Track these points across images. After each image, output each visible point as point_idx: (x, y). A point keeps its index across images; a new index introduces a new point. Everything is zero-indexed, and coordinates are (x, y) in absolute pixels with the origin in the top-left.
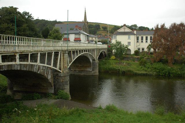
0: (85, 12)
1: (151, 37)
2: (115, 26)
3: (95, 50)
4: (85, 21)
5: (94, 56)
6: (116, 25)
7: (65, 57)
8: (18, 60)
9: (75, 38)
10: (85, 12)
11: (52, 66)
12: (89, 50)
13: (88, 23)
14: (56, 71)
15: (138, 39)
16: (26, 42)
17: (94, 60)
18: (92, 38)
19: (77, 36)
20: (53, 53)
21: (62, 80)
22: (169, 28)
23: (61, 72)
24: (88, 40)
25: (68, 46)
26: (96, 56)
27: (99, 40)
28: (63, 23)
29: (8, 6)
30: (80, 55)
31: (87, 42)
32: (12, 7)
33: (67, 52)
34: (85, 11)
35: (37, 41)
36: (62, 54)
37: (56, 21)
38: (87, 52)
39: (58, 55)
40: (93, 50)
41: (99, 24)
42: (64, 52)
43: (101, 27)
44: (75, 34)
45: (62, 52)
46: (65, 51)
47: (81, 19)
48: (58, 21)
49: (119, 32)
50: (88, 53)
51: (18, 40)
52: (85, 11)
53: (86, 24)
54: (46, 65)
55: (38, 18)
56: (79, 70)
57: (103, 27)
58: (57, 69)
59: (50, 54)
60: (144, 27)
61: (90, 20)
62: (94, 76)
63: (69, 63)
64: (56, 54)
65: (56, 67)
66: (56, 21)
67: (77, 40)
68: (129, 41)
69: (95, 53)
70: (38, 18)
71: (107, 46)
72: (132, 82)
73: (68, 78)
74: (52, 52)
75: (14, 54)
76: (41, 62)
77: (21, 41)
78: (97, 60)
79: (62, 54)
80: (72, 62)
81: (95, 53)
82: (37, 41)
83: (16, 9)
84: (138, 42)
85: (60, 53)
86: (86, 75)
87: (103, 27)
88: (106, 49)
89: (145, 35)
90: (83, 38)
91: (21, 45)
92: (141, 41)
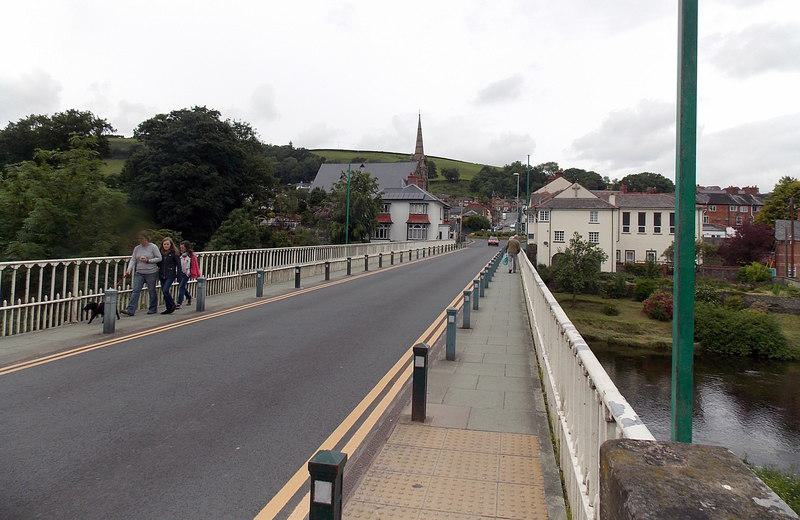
0: (420, 129)
1: (672, 215)
2: (486, 168)
9: (412, 216)
10: (420, 129)
15: (626, 219)
16: (789, 255)
19: (419, 210)
29: (189, 106)
32: (204, 109)
37: (290, 146)
44: (412, 202)
47: (411, 150)
48: (296, 146)
49: (562, 200)
57: (444, 172)
60: (583, 171)
61: (429, 151)
66: (290, 146)
67: (418, 223)
68: (594, 228)
83: (215, 113)
84: (626, 230)
86: (621, 345)
87: (444, 172)
89: (651, 208)
92: (653, 227)
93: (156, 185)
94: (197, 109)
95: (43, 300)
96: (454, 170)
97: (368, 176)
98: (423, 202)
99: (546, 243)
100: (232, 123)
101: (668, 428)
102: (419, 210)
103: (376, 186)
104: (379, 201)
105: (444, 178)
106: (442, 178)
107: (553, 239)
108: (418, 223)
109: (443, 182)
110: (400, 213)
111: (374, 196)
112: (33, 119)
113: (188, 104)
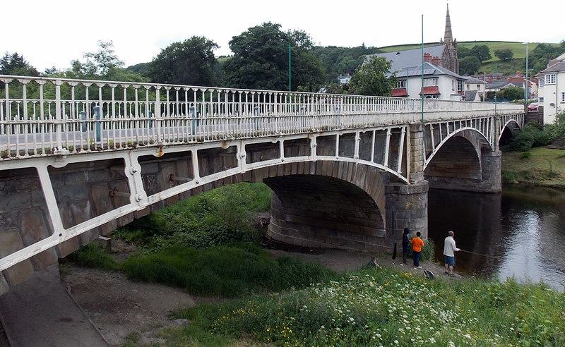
0: (448, 21)
2: (541, 46)
3: (490, 119)
4: (449, 43)
5: (487, 138)
6: (541, 42)
7: (416, 141)
8: (314, 150)
9: (424, 89)
11: (385, 167)
12: (475, 121)
13: (455, 43)
14: (394, 178)
17: (486, 150)
18: (478, 86)
19: (430, 83)
20: (389, 133)
21: (408, 204)
22: (231, 54)
23: (405, 183)
24: (460, 92)
25: (422, 113)
26: (493, 136)
27: (488, 90)
28: (381, 50)
29: (260, 24)
30: (452, 135)
31: (458, 98)
32: (270, 24)
33: (421, 129)
34: (448, 11)
35: (302, 100)
36: (408, 135)
38: (469, 125)
39: (399, 135)
40: (484, 121)
41: (484, 44)
42: (414, 128)
43: (492, 54)
45: (408, 129)
46: (418, 126)
47: (435, 34)
48: (368, 46)
50: (471, 128)
51: (278, 101)
52: (448, 11)
53: (451, 47)
54: (372, 163)
55: (320, 43)
56: (441, 175)
57: (497, 53)
58: (398, 173)
59: (381, 134)
60: (335, 47)
61: (460, 35)
62: (487, 196)
63: (425, 159)
64: (396, 133)
65: (395, 168)
69: (489, 129)
70: (320, 43)
71: (522, 107)
72: (69, 176)
73: (424, 200)
74: (386, 130)
75: (306, 137)
76: (361, 157)
77: (240, 103)
78: (498, 148)
79: (408, 135)
80: (432, 156)
81: (489, 129)
82: (302, 100)
83: (276, 26)
85: (403, 130)
87: (497, 53)
88: (520, 115)
90: (446, 86)
91: (275, 114)
93: (237, 79)
94: (265, 24)
95: (198, 117)
96: (508, 50)
97: (384, 59)
98: (434, 76)
99: (552, 105)
100: (292, 31)
101: (230, 65)
102: (430, 83)
103: (389, 67)
104: (394, 79)
105: (497, 59)
106: (495, 59)
107: (560, 100)
108: (430, 94)
109: (498, 62)
110: (414, 87)
111: (388, 76)
112: (174, 45)
113: (259, 23)
